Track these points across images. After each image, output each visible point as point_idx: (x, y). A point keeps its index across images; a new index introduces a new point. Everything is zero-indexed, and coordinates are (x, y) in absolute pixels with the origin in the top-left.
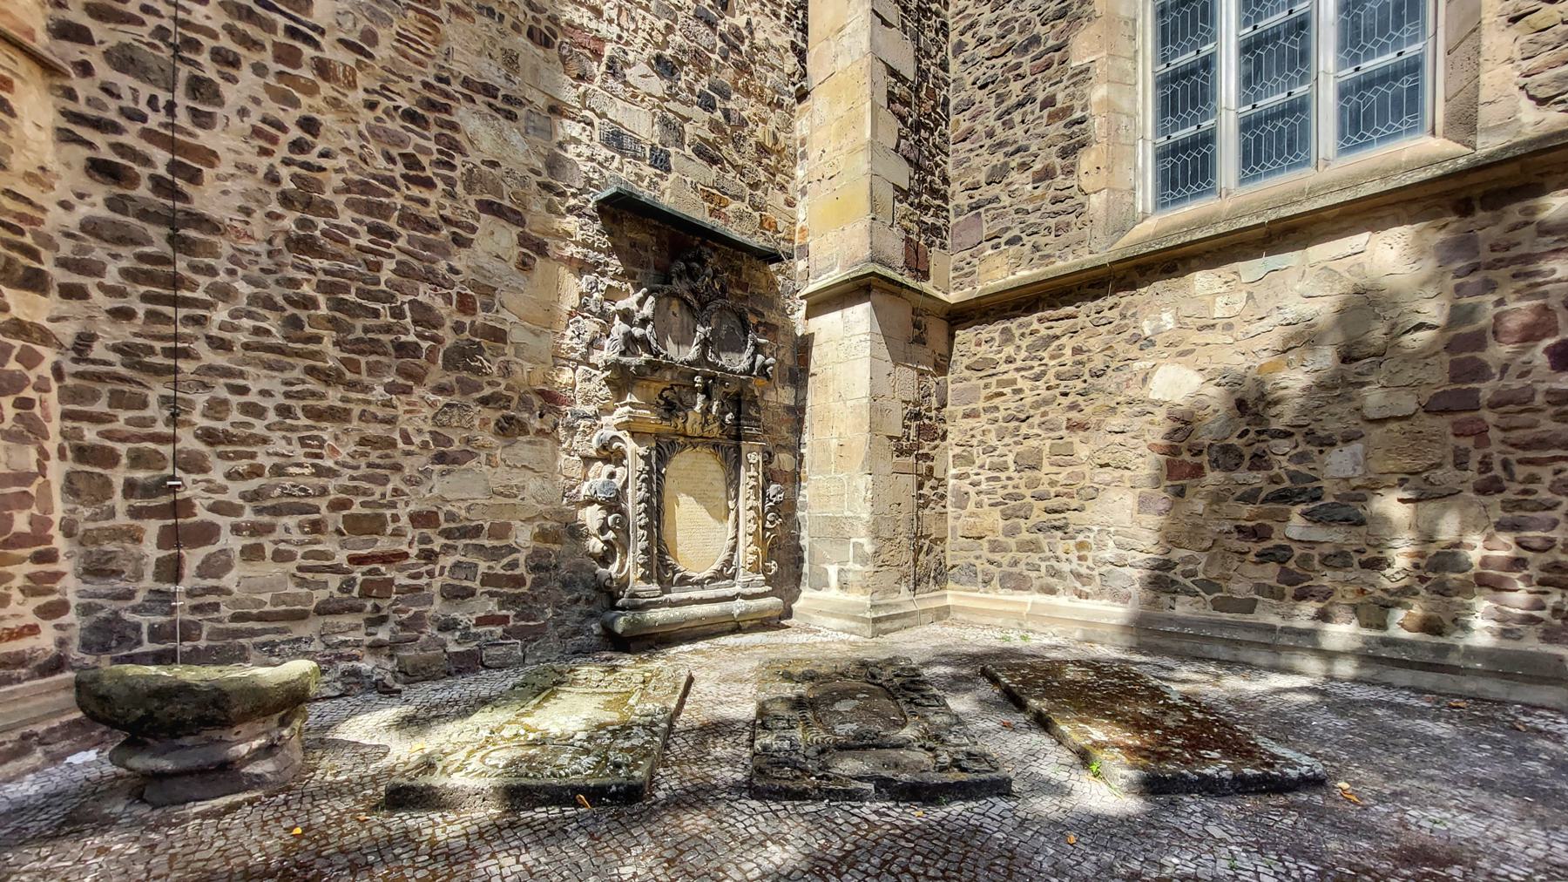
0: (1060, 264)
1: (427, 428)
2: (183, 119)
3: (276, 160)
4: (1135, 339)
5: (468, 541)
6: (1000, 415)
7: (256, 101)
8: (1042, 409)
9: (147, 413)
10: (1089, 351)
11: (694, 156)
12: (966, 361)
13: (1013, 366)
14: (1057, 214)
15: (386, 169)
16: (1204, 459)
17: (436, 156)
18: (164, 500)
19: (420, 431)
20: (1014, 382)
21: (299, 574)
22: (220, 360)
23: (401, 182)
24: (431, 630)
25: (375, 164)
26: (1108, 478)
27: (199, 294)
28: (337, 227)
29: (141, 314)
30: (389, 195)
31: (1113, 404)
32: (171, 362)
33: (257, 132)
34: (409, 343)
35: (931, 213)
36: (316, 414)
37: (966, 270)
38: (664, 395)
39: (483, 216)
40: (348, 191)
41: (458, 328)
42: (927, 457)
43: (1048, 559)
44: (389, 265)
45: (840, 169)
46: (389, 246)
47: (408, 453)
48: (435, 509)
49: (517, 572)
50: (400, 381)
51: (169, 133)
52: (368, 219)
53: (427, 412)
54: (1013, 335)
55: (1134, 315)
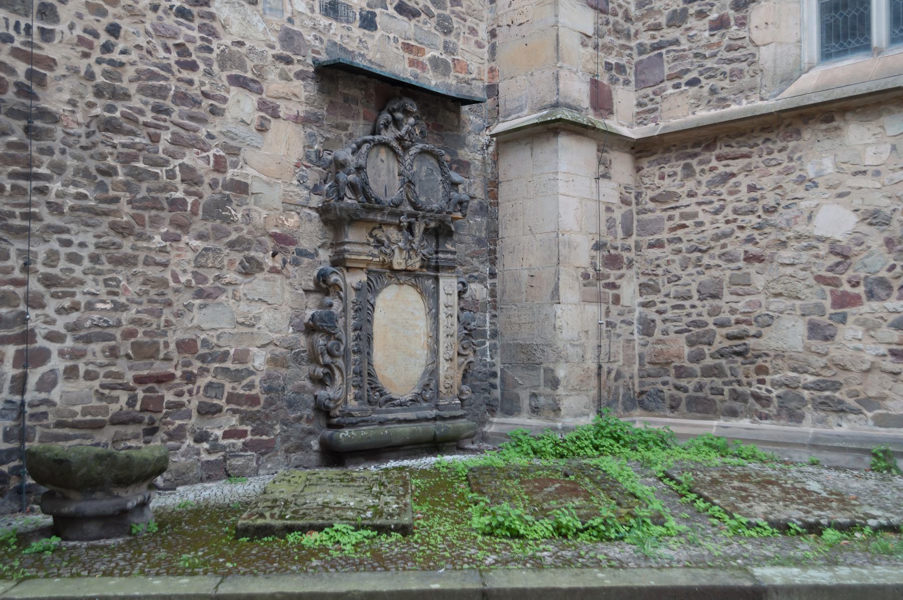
0: (734, 107)
1: (190, 268)
2: (36, 38)
3: (92, 60)
4: (801, 180)
5: (217, 365)
6: (683, 246)
7: (80, 16)
8: (722, 241)
9: (9, 263)
10: (762, 189)
11: (396, 14)
12: (651, 194)
13: (694, 200)
14: (731, 61)
15: (164, 58)
16: (861, 290)
17: (199, 43)
18: (17, 330)
19: (185, 271)
20: (695, 215)
21: (101, 391)
22: (55, 221)
23: (175, 68)
24: (189, 441)
25: (157, 55)
26: (782, 307)
27: (43, 170)
28: (130, 108)
29: (8, 187)
30: (167, 79)
31: (783, 239)
32: (25, 223)
33: (81, 41)
34: (179, 199)
35: (614, 53)
36: (117, 261)
37: (650, 106)
38: (374, 233)
39: (233, 88)
40: (138, 79)
41: (213, 185)
42: (613, 286)
43: (731, 383)
44: (166, 136)
45: (529, 18)
46: (165, 121)
47: (177, 291)
48: (194, 337)
49: (253, 392)
50: (172, 230)
51: (29, 49)
52: (152, 101)
53: (190, 256)
54: (694, 171)
55: (800, 158)
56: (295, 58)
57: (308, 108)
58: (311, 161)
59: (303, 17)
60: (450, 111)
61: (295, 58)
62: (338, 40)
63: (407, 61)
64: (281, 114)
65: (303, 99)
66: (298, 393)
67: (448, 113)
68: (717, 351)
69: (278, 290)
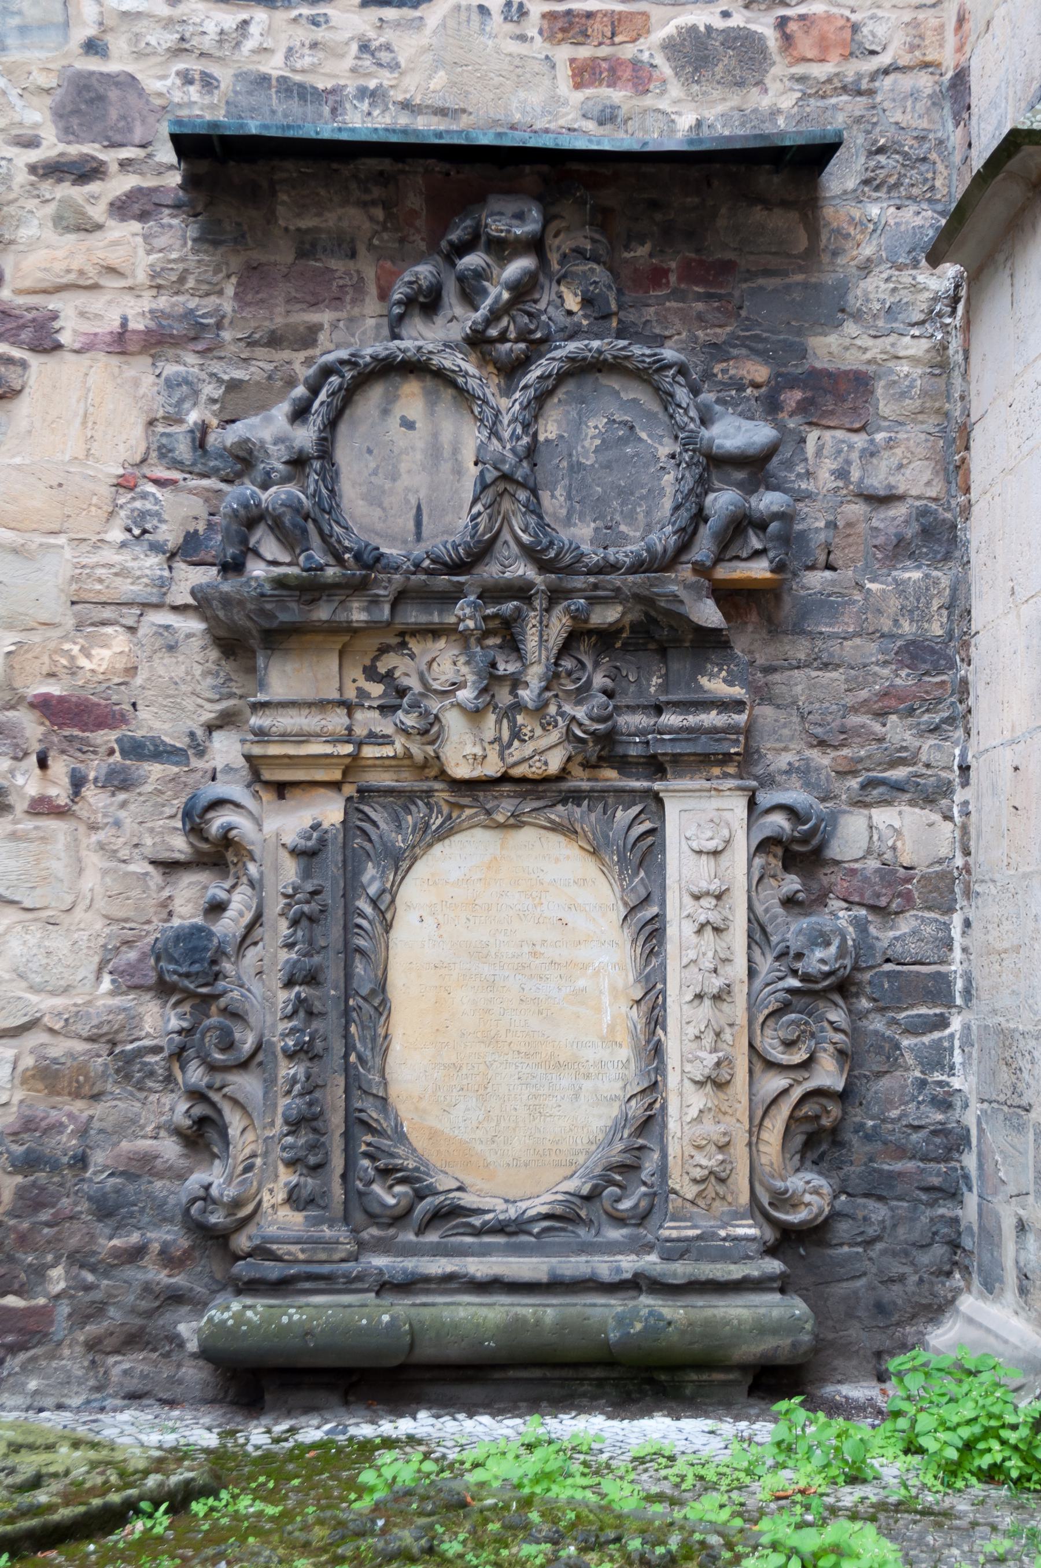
56: (111, 157)
57: (163, 302)
58: (177, 464)
59: (140, 27)
60: (767, 204)
61: (111, 157)
62: (274, 66)
63: (564, 72)
64: (64, 338)
65: (141, 276)
66: (129, 1176)
67: (758, 214)
68: (330, 1191)
69: (59, 867)
